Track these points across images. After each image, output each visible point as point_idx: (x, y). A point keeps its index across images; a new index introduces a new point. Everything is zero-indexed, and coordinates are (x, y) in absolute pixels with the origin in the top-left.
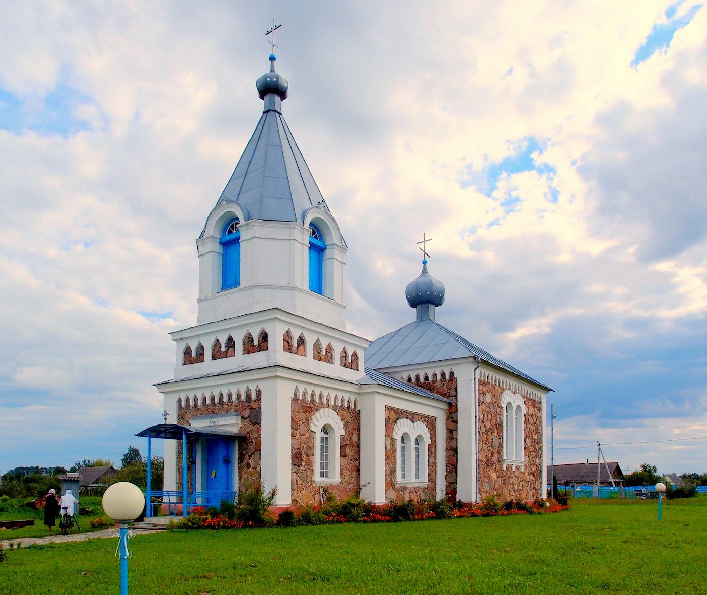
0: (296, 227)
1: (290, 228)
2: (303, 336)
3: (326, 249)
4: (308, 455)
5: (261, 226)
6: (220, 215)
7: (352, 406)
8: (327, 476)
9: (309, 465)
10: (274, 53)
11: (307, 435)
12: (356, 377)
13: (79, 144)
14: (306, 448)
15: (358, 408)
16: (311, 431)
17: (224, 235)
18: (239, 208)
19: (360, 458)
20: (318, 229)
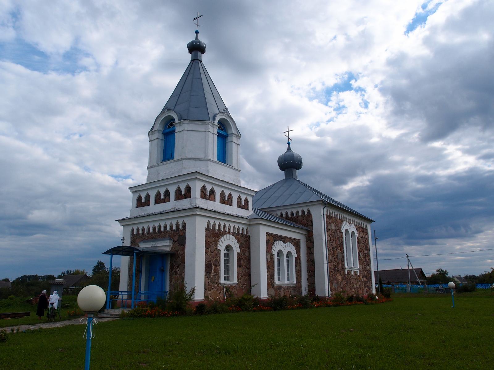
0: (210, 124)
3: (228, 136)
4: (216, 265)
5: (188, 123)
8: (228, 280)
9: (217, 272)
11: (216, 252)
13: (81, 79)
15: (249, 234)
16: (218, 249)
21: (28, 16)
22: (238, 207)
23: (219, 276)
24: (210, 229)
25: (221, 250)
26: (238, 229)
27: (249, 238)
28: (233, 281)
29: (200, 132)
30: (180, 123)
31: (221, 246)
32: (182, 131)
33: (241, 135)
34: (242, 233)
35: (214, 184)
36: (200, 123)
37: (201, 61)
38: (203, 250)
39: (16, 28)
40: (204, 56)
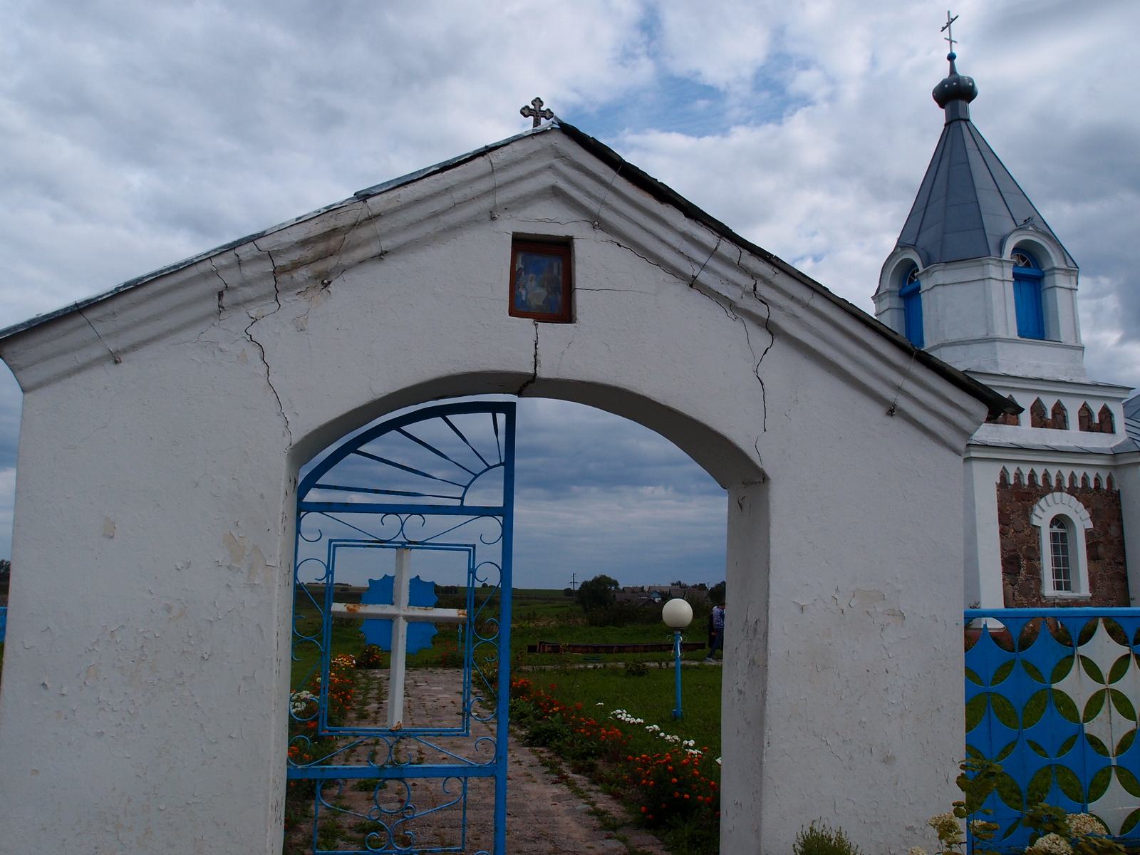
0: (991, 262)
1: (983, 265)
2: (1013, 398)
3: (1043, 276)
4: (1029, 559)
5: (943, 270)
6: (896, 264)
7: (1105, 486)
8: (1068, 588)
9: (1035, 573)
10: (954, 51)
11: (1027, 532)
12: (1110, 443)
13: (798, 128)
14: (1026, 549)
15: (1116, 487)
16: (1034, 526)
17: (904, 286)
18: (915, 253)
19: (1125, 561)
20: (1030, 254)
21: (675, 21)
22: (1082, 428)
23: (1041, 581)
24: (1010, 484)
25: (1040, 527)
26: (1085, 479)
27: (1117, 495)
28: (1079, 592)
29: (973, 284)
30: (927, 271)
31: (1041, 518)
32: (933, 287)
33: (1078, 267)
34: (1098, 487)
35: (1013, 388)
36: (974, 264)
37: (969, 120)
38: (996, 528)
39: (653, 55)
40: (973, 106)
